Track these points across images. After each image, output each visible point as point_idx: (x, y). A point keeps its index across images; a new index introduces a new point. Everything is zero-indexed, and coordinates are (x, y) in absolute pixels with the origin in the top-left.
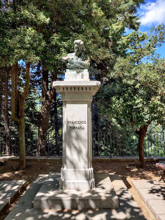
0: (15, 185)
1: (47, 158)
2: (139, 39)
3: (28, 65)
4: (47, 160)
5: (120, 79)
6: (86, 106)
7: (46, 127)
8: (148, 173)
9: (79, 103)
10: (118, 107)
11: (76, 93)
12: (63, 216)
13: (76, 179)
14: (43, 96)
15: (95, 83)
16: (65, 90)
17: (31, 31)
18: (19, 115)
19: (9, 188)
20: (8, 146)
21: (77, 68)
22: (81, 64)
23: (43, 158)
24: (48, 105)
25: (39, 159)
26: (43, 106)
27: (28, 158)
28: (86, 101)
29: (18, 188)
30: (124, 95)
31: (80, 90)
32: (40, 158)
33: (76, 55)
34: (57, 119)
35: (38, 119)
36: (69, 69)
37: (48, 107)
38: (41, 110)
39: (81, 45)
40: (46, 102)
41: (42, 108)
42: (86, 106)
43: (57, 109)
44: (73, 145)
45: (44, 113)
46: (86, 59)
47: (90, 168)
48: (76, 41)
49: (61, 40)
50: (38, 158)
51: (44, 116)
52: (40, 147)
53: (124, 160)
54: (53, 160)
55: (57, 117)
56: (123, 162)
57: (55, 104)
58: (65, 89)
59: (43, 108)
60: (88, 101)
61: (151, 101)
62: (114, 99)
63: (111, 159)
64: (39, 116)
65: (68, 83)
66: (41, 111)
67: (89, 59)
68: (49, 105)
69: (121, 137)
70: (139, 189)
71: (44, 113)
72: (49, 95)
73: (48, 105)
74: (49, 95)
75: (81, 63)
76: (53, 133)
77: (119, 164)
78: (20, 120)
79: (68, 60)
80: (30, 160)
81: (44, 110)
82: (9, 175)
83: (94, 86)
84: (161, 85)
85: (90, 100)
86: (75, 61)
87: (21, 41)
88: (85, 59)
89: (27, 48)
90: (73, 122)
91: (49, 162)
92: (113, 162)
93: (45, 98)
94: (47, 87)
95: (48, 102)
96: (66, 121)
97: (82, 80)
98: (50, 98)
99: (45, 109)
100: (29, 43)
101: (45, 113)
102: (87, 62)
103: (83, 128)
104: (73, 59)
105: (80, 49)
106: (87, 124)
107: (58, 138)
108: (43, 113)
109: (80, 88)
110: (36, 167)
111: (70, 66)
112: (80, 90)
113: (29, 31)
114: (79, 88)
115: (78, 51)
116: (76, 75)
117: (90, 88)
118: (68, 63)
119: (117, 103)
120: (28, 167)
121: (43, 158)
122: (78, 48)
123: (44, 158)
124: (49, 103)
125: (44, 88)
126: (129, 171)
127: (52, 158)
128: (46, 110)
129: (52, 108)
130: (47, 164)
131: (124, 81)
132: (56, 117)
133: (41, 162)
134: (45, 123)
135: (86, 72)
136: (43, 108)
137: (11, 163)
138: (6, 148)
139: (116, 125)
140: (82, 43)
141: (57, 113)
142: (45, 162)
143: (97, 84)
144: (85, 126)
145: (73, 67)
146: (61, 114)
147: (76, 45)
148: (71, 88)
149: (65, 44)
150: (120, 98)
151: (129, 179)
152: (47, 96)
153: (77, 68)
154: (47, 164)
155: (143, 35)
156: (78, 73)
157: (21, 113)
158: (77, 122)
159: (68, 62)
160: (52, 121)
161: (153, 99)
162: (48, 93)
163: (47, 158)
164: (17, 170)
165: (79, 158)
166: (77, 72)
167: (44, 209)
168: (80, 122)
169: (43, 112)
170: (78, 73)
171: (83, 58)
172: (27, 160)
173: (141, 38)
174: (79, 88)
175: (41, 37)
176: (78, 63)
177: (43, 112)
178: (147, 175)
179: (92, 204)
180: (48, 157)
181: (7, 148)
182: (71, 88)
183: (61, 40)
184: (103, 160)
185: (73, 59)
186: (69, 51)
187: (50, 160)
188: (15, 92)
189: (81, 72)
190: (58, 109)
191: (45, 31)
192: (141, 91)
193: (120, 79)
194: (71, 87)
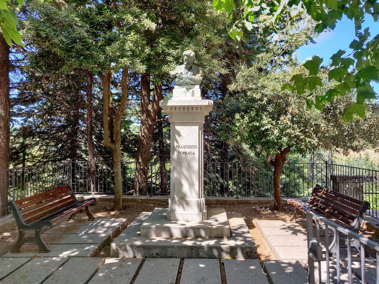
0: (114, 222)
1: (149, 198)
2: (292, 19)
3: (125, 72)
4: (150, 200)
5: (245, 92)
6: (197, 128)
7: (148, 156)
8: (282, 216)
9: (189, 125)
10: (243, 128)
11: (187, 113)
12: (172, 241)
13: (188, 214)
14: (142, 112)
15: (206, 102)
16: (173, 110)
17: (133, 36)
18: (114, 139)
19: (108, 224)
20: (93, 183)
21: (187, 84)
22: (191, 79)
23: (144, 198)
24: (149, 125)
25: (140, 199)
26: (142, 127)
27: (124, 198)
28: (197, 123)
29: (118, 225)
30: (250, 112)
31: (190, 110)
32: (140, 198)
33: (186, 68)
34: (163, 146)
35: (134, 146)
36: (178, 85)
37: (150, 128)
38: (140, 132)
39: (192, 57)
40: (148, 121)
41: (141, 130)
42: (197, 128)
43: (164, 131)
44: (184, 175)
45: (145, 136)
46: (198, 72)
47: (202, 198)
48: (186, 52)
49: (168, 45)
50: (137, 198)
51: (145, 141)
52: (138, 186)
53: (255, 201)
54: (158, 200)
55: (163, 143)
56: (255, 204)
57: (160, 123)
58: (173, 108)
59: (143, 129)
60: (199, 123)
61: (279, 122)
62: (237, 116)
63: (237, 199)
64: (137, 141)
65: (176, 102)
66: (140, 134)
67: (201, 72)
68: (152, 125)
69: (255, 172)
70: (262, 228)
71: (145, 136)
72: (152, 111)
73: (149, 125)
74: (152, 111)
75: (191, 78)
76: (156, 168)
77: (247, 207)
78: (115, 146)
79: (177, 75)
80: (127, 200)
81: (144, 133)
82: (104, 215)
83: (205, 105)
84: (292, 101)
85: (202, 122)
86: (184, 76)
87: (122, 49)
88: (196, 72)
89: (128, 55)
90: (182, 147)
91: (152, 203)
92: (240, 203)
93: (145, 115)
94: (149, 98)
95: (149, 121)
96: (192, 191)
97: (193, 98)
98: (152, 114)
99: (145, 130)
100: (131, 50)
101: (146, 136)
102: (198, 77)
103: (194, 153)
104: (181, 73)
105: (191, 61)
106: (198, 149)
107: (164, 175)
108: (143, 136)
109: (189, 108)
110: (135, 207)
111: (178, 82)
112: (190, 110)
113: (132, 36)
114: (188, 108)
115: (188, 63)
116: (185, 92)
117: (201, 107)
118: (177, 79)
119: (241, 122)
120: (125, 208)
121: (144, 198)
122: (188, 60)
123: (146, 198)
124: (151, 122)
125: (144, 100)
126: (259, 213)
127: (157, 198)
128: (147, 132)
129: (155, 129)
130: (151, 205)
131: (249, 93)
132: (161, 143)
133: (141, 202)
134: (145, 152)
135: (197, 89)
136: (143, 129)
137: (102, 203)
138: (90, 186)
139: (249, 154)
140: (193, 54)
141: (162, 136)
142: (148, 203)
143: (209, 103)
144: (196, 151)
145: (183, 83)
146: (168, 138)
147: (185, 57)
148: (180, 108)
149: (174, 52)
150: (245, 117)
151: (255, 221)
152: (148, 112)
153: (187, 84)
154: (151, 205)
155: (299, 13)
156: (188, 89)
157: (117, 136)
158: (186, 147)
159: (176, 77)
160: (155, 148)
161: (282, 118)
162: (150, 107)
163: (149, 198)
164: (113, 210)
165: (191, 191)
166: (187, 89)
167: (151, 236)
168: (190, 147)
169: (143, 135)
170: (188, 89)
171: (194, 71)
172: (124, 200)
173: (295, 18)
174: (188, 108)
175: (144, 42)
176: (187, 78)
177: (143, 135)
178: (281, 217)
179: (203, 233)
180: (151, 196)
181: (92, 186)
182: (180, 108)
183: (168, 45)
184: (225, 201)
185: (181, 73)
186: (178, 60)
187: (153, 200)
188: (109, 109)
189: (191, 89)
190: (164, 130)
191: (150, 38)
192: (270, 109)
193: (245, 92)
194: (180, 107)
